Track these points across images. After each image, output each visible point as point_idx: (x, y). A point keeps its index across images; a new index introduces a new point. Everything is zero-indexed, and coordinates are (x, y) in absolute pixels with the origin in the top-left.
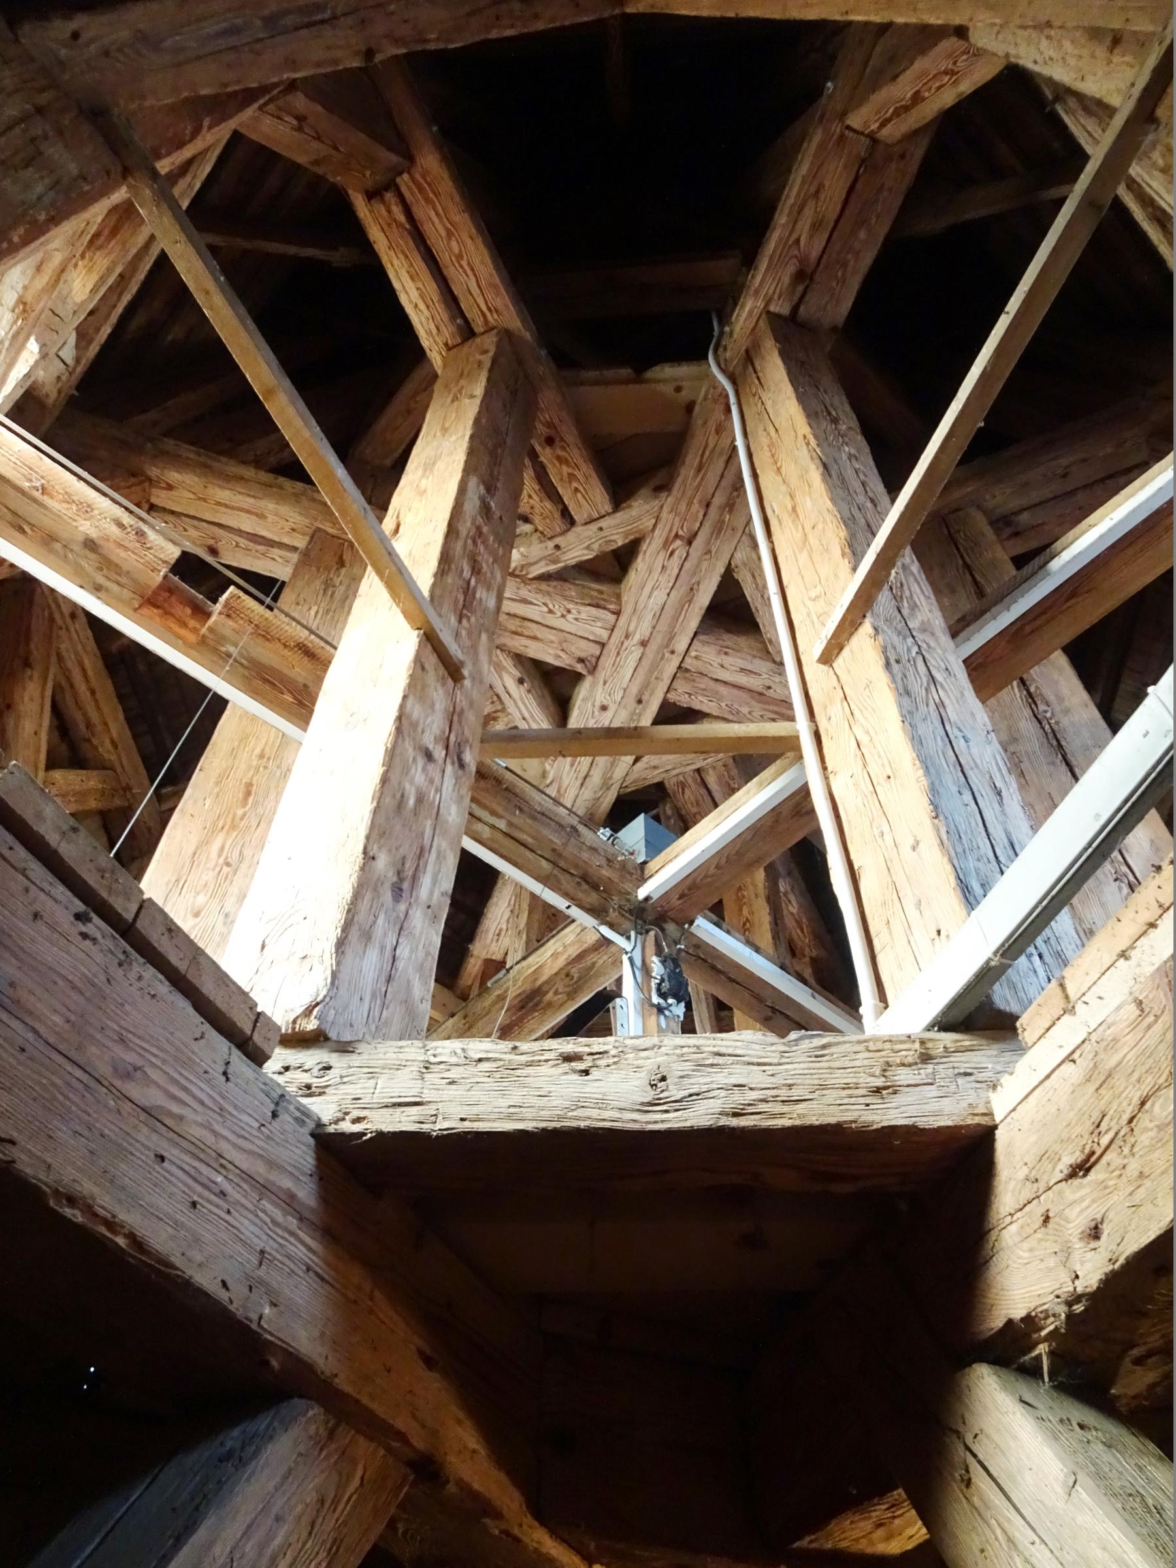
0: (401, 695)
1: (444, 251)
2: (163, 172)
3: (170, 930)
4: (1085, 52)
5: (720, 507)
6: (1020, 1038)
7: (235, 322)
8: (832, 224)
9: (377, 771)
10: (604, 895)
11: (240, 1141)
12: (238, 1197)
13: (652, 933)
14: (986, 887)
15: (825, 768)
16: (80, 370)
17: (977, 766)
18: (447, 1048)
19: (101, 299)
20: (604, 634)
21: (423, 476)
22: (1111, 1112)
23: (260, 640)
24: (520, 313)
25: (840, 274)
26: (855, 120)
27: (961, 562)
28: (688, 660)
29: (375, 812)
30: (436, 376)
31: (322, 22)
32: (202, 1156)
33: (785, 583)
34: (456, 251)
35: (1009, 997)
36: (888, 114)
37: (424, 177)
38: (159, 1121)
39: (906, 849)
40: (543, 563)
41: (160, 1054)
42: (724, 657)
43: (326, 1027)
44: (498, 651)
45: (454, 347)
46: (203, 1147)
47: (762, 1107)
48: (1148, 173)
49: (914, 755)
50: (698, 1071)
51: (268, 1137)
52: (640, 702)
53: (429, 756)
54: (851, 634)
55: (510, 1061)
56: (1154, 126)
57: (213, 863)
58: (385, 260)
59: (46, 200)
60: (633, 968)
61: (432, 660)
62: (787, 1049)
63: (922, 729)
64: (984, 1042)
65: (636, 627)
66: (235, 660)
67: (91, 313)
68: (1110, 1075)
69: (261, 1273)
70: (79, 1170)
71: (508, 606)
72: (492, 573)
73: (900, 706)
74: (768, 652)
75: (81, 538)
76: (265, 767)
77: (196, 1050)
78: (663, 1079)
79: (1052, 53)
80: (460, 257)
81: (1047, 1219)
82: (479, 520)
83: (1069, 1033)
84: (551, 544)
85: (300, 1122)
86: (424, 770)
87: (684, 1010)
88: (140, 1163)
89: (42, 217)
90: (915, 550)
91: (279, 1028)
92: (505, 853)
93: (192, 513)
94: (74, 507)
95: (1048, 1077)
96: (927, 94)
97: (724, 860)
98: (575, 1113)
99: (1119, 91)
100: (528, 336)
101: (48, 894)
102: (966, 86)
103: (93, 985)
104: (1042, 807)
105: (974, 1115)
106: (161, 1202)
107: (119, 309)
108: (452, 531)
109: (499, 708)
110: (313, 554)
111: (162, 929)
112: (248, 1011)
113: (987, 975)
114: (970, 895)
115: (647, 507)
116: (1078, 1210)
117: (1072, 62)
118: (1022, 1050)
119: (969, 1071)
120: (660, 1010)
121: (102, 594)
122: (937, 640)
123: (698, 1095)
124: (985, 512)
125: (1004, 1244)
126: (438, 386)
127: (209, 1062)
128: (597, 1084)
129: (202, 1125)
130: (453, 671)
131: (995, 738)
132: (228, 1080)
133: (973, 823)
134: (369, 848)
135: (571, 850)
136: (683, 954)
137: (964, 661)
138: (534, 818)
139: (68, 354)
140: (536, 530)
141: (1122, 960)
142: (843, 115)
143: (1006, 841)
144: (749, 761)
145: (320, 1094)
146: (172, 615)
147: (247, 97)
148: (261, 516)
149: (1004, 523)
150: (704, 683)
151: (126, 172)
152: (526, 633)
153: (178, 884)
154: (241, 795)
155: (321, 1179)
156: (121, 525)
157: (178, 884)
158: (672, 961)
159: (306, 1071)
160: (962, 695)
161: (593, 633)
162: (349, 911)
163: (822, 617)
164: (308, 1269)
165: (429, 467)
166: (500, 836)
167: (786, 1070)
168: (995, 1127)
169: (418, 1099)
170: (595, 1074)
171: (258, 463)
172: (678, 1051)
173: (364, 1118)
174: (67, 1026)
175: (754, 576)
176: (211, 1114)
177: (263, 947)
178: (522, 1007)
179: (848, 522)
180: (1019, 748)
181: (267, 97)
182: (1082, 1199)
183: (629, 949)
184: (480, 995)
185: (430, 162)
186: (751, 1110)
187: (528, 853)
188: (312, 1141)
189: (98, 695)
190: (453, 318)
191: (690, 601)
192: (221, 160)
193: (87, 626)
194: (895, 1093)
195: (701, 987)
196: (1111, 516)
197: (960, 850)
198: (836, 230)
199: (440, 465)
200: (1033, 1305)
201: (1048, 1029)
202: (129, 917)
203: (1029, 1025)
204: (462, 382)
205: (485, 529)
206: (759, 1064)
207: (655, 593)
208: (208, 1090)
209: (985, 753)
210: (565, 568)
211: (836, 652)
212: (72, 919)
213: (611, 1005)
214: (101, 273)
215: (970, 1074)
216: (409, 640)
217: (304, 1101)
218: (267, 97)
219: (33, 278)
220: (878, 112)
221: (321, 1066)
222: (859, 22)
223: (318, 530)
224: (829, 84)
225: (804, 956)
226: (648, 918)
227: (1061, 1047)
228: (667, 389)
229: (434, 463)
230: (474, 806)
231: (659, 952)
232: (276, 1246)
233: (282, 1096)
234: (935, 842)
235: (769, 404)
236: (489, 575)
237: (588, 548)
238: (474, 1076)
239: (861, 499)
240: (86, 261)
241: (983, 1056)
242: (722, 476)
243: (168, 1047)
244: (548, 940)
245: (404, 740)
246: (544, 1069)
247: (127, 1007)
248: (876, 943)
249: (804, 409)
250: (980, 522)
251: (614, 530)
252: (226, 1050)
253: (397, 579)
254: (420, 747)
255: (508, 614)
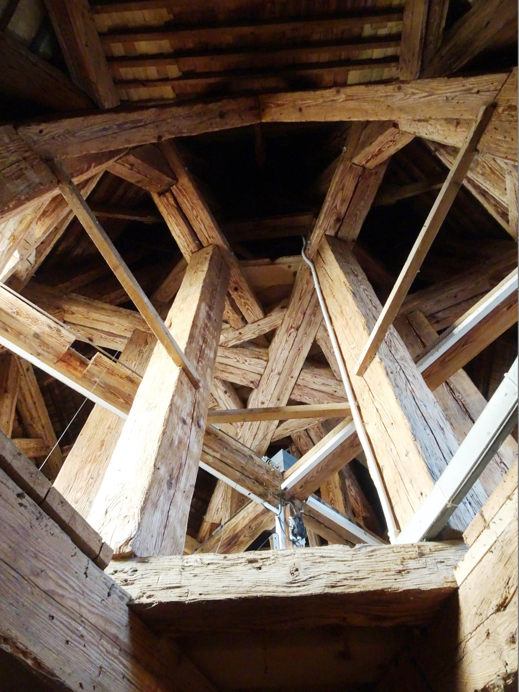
0: (172, 395)
1: (190, 215)
2: (76, 183)
3: (62, 502)
4: (445, 129)
5: (309, 315)
6: (465, 542)
7: (102, 239)
8: (350, 199)
9: (161, 429)
10: (266, 488)
11: (91, 609)
12: (89, 638)
13: (288, 505)
14: (441, 471)
15: (363, 422)
16: (37, 266)
17: (431, 417)
18: (194, 558)
19: (46, 237)
20: (262, 371)
21: (182, 303)
22: (513, 576)
23: (110, 376)
24: (222, 238)
25: (354, 219)
26: (356, 161)
27: (415, 334)
28: (299, 380)
29: (160, 447)
30: (187, 264)
31: (141, 126)
32: (72, 616)
33: (340, 343)
34: (195, 214)
35: (458, 524)
36: (369, 158)
37: (182, 186)
38: (52, 598)
39: (403, 458)
40: (234, 340)
41: (55, 564)
42: (315, 379)
43: (135, 550)
44: (215, 379)
45: (195, 252)
46: (72, 611)
47: (345, 582)
48: (477, 176)
49: (403, 413)
50: (313, 565)
51: (106, 606)
52: (279, 400)
53: (184, 422)
54: (370, 362)
55: (223, 564)
56: (477, 153)
57: (85, 477)
58: (166, 219)
59: (24, 192)
60: (280, 522)
61: (185, 380)
62: (355, 553)
63: (405, 402)
64: (448, 546)
65: (276, 367)
66: (98, 384)
67: (42, 243)
68: (510, 557)
69: (99, 679)
70: (11, 623)
71: (218, 359)
72: (212, 343)
73: (395, 392)
74: (334, 376)
75: (32, 333)
76: (111, 433)
77: (72, 561)
78: (297, 570)
79: (432, 130)
80: (197, 217)
81: (488, 634)
82: (206, 321)
83: (488, 538)
84: (237, 332)
85: (122, 598)
86: (182, 428)
87: (305, 542)
88: (41, 619)
89: (23, 198)
90: (395, 326)
91: (113, 551)
92: (220, 469)
93: (82, 324)
94: (30, 320)
95: (480, 561)
96: (384, 150)
97: (319, 470)
98: (255, 589)
99: (461, 141)
100: (225, 247)
101: (5, 485)
102: (400, 145)
103: (24, 529)
104: (461, 435)
105: (447, 582)
106: (51, 641)
107: (54, 242)
108: (194, 325)
109: (216, 404)
110: (134, 340)
111: (58, 501)
112: (98, 542)
113: (446, 512)
114: (434, 475)
115: (278, 315)
116: (503, 628)
117: (441, 132)
118: (467, 549)
119: (442, 560)
120: (294, 542)
121: (40, 357)
122: (408, 364)
123: (314, 577)
124: (424, 313)
125: (468, 649)
126: (188, 268)
127: (78, 567)
128: (265, 574)
129: (72, 600)
130: (195, 384)
131: (438, 405)
132: (87, 577)
133: (432, 443)
134: (157, 464)
135: (250, 467)
136: (303, 515)
137: (422, 373)
138: (233, 453)
139: (32, 259)
140: (231, 327)
141: (509, 500)
142: (351, 158)
143: (448, 451)
144: (329, 422)
145: (132, 584)
146: (71, 365)
147: (111, 154)
148: (112, 324)
149: (432, 317)
150: (306, 390)
151: (59, 182)
152: (228, 371)
153: (69, 488)
154: (99, 446)
155: (131, 628)
156: (50, 327)
157: (69, 488)
158: (298, 518)
159: (125, 573)
160: (422, 387)
161: (257, 370)
162: (147, 493)
163: (357, 356)
164: (124, 677)
165: (184, 300)
166: (217, 461)
167: (355, 564)
168: (458, 588)
169: (179, 585)
170: (264, 569)
171: (111, 303)
172: (303, 556)
173: (153, 595)
174: (9, 550)
175: (326, 343)
176: (78, 594)
177: (106, 513)
178: (229, 544)
179: (366, 315)
180: (449, 413)
181: (119, 157)
182: (504, 622)
183: (278, 513)
184: (209, 539)
185: (185, 181)
186: (339, 584)
187: (230, 469)
188: (127, 608)
189: (37, 404)
190: (194, 241)
191: (299, 355)
192: (99, 183)
193: (34, 374)
194: (408, 572)
195: (312, 531)
196: (478, 309)
197: (427, 455)
198: (352, 201)
199: (189, 298)
200: (487, 681)
201: (478, 537)
202: (43, 495)
203: (468, 536)
204: (199, 266)
205: (209, 325)
206: (342, 561)
207: (284, 352)
208: (77, 581)
209: (434, 411)
210: (244, 342)
211: (364, 370)
212: (16, 497)
213: (270, 538)
214: (47, 226)
215: (443, 562)
216: (175, 371)
217: (124, 588)
218: (119, 157)
219: (18, 226)
220: (365, 157)
221: (132, 570)
222: (356, 121)
223: (137, 329)
224: (345, 148)
225: (359, 516)
226: (287, 498)
227: (485, 545)
228: (285, 267)
229: (186, 298)
230: (205, 447)
231: (292, 514)
232: (107, 664)
233: (113, 585)
234: (416, 452)
235: (328, 271)
236: (210, 344)
237: (254, 333)
238: (206, 572)
239: (370, 306)
240: (41, 222)
241: (448, 552)
242: (310, 302)
243: (59, 560)
244: (240, 511)
245: (173, 415)
246: (240, 568)
247: (39, 540)
248: (393, 501)
249: (343, 272)
250: (422, 317)
251: (265, 325)
252: (87, 561)
253: (170, 345)
254: (180, 418)
255: (219, 363)
